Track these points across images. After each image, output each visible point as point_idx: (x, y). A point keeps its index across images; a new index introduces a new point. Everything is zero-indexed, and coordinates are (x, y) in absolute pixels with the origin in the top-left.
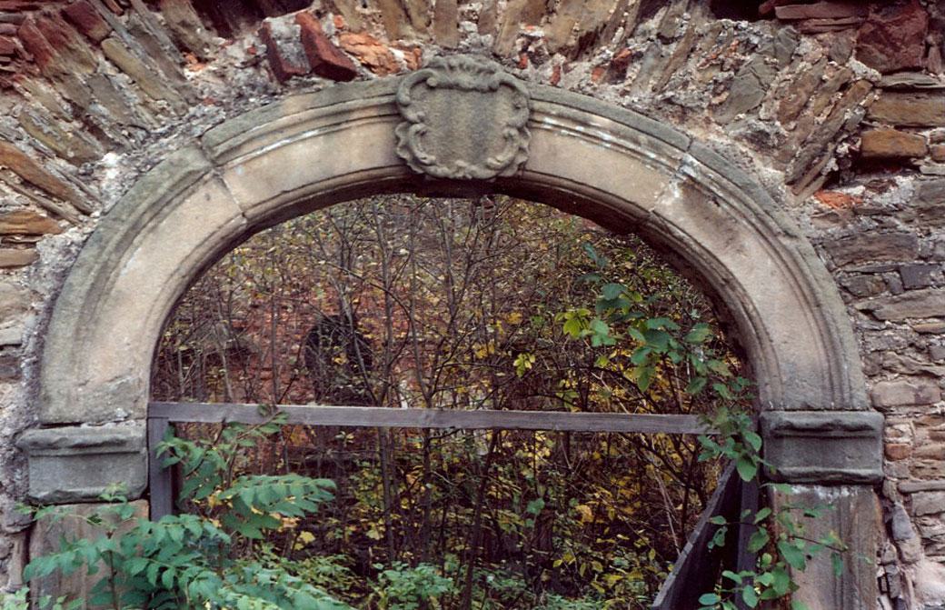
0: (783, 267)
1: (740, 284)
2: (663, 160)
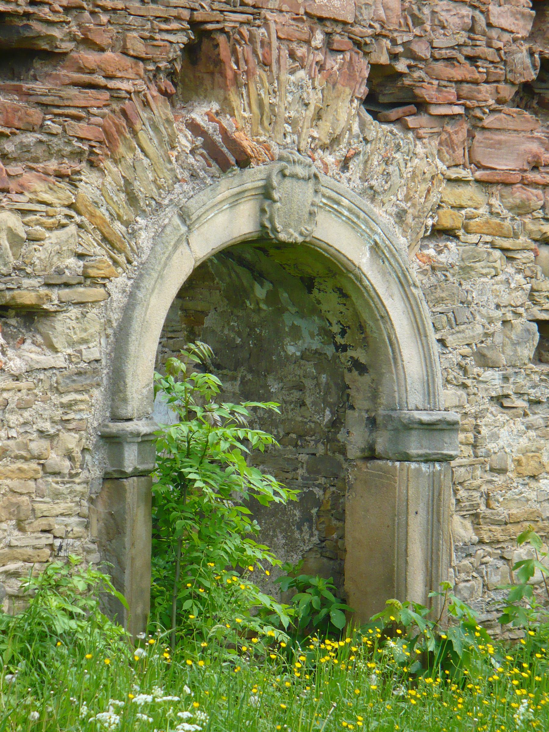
0: (409, 310)
1: (390, 319)
2: (368, 231)
